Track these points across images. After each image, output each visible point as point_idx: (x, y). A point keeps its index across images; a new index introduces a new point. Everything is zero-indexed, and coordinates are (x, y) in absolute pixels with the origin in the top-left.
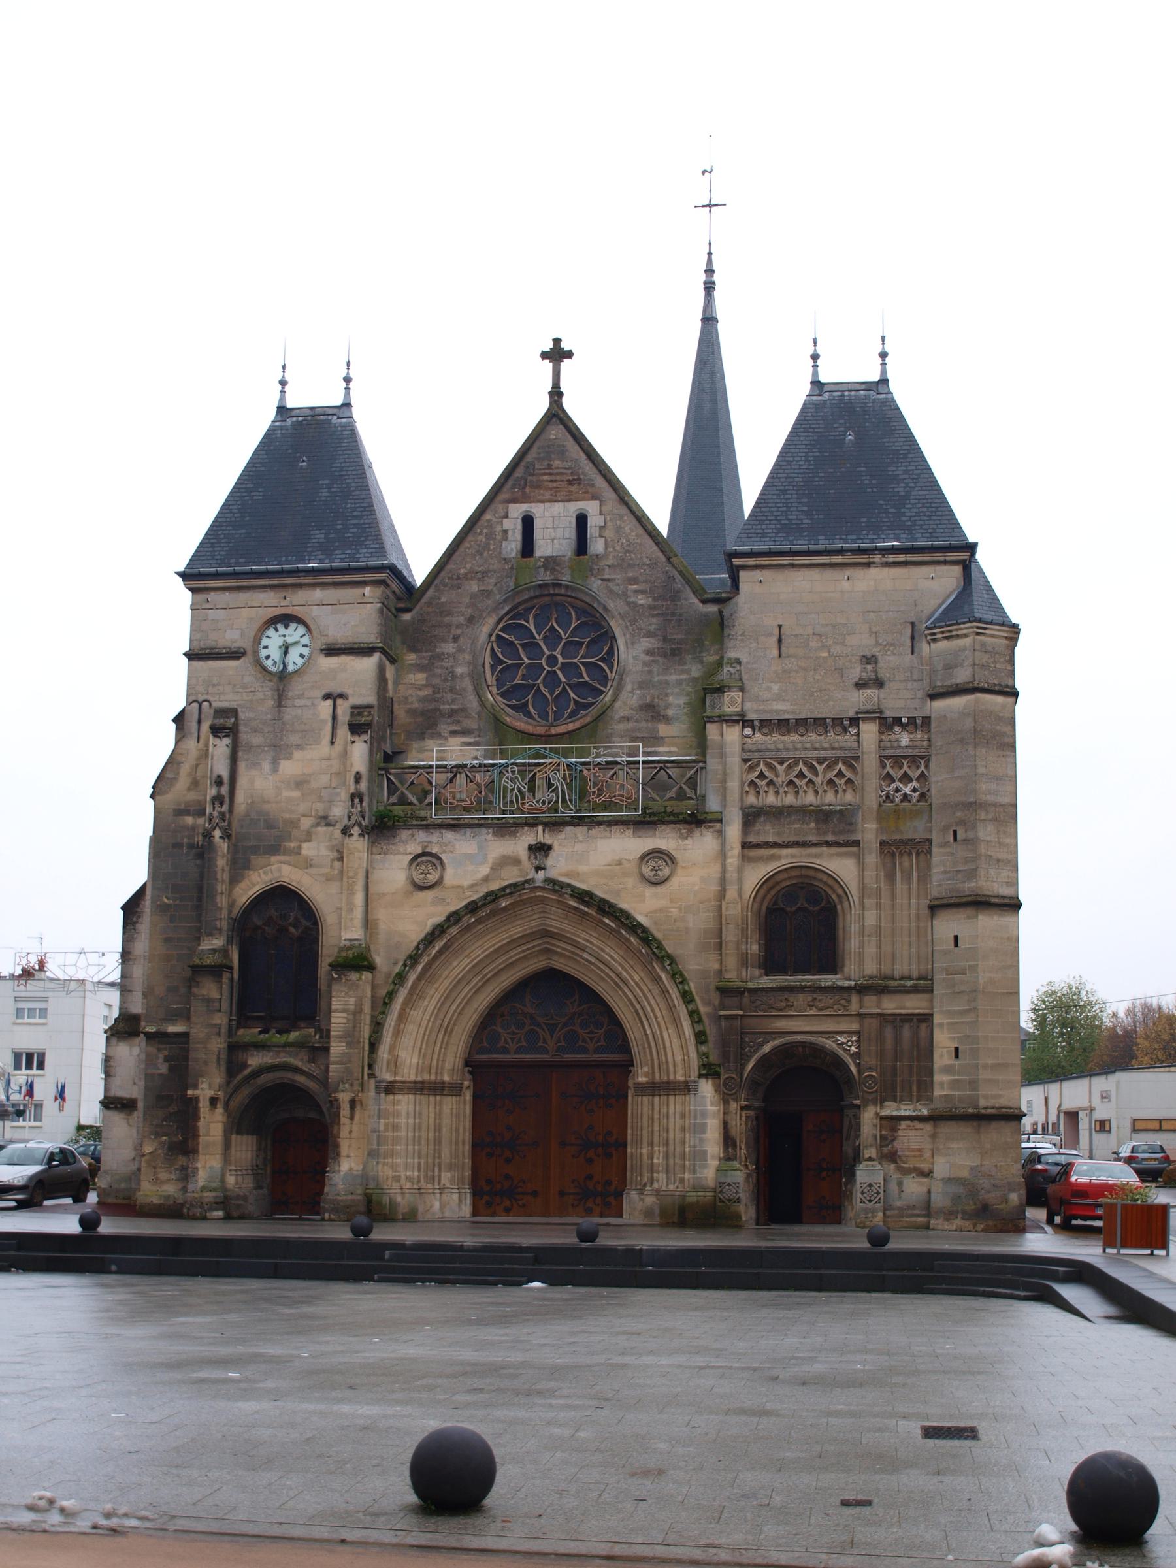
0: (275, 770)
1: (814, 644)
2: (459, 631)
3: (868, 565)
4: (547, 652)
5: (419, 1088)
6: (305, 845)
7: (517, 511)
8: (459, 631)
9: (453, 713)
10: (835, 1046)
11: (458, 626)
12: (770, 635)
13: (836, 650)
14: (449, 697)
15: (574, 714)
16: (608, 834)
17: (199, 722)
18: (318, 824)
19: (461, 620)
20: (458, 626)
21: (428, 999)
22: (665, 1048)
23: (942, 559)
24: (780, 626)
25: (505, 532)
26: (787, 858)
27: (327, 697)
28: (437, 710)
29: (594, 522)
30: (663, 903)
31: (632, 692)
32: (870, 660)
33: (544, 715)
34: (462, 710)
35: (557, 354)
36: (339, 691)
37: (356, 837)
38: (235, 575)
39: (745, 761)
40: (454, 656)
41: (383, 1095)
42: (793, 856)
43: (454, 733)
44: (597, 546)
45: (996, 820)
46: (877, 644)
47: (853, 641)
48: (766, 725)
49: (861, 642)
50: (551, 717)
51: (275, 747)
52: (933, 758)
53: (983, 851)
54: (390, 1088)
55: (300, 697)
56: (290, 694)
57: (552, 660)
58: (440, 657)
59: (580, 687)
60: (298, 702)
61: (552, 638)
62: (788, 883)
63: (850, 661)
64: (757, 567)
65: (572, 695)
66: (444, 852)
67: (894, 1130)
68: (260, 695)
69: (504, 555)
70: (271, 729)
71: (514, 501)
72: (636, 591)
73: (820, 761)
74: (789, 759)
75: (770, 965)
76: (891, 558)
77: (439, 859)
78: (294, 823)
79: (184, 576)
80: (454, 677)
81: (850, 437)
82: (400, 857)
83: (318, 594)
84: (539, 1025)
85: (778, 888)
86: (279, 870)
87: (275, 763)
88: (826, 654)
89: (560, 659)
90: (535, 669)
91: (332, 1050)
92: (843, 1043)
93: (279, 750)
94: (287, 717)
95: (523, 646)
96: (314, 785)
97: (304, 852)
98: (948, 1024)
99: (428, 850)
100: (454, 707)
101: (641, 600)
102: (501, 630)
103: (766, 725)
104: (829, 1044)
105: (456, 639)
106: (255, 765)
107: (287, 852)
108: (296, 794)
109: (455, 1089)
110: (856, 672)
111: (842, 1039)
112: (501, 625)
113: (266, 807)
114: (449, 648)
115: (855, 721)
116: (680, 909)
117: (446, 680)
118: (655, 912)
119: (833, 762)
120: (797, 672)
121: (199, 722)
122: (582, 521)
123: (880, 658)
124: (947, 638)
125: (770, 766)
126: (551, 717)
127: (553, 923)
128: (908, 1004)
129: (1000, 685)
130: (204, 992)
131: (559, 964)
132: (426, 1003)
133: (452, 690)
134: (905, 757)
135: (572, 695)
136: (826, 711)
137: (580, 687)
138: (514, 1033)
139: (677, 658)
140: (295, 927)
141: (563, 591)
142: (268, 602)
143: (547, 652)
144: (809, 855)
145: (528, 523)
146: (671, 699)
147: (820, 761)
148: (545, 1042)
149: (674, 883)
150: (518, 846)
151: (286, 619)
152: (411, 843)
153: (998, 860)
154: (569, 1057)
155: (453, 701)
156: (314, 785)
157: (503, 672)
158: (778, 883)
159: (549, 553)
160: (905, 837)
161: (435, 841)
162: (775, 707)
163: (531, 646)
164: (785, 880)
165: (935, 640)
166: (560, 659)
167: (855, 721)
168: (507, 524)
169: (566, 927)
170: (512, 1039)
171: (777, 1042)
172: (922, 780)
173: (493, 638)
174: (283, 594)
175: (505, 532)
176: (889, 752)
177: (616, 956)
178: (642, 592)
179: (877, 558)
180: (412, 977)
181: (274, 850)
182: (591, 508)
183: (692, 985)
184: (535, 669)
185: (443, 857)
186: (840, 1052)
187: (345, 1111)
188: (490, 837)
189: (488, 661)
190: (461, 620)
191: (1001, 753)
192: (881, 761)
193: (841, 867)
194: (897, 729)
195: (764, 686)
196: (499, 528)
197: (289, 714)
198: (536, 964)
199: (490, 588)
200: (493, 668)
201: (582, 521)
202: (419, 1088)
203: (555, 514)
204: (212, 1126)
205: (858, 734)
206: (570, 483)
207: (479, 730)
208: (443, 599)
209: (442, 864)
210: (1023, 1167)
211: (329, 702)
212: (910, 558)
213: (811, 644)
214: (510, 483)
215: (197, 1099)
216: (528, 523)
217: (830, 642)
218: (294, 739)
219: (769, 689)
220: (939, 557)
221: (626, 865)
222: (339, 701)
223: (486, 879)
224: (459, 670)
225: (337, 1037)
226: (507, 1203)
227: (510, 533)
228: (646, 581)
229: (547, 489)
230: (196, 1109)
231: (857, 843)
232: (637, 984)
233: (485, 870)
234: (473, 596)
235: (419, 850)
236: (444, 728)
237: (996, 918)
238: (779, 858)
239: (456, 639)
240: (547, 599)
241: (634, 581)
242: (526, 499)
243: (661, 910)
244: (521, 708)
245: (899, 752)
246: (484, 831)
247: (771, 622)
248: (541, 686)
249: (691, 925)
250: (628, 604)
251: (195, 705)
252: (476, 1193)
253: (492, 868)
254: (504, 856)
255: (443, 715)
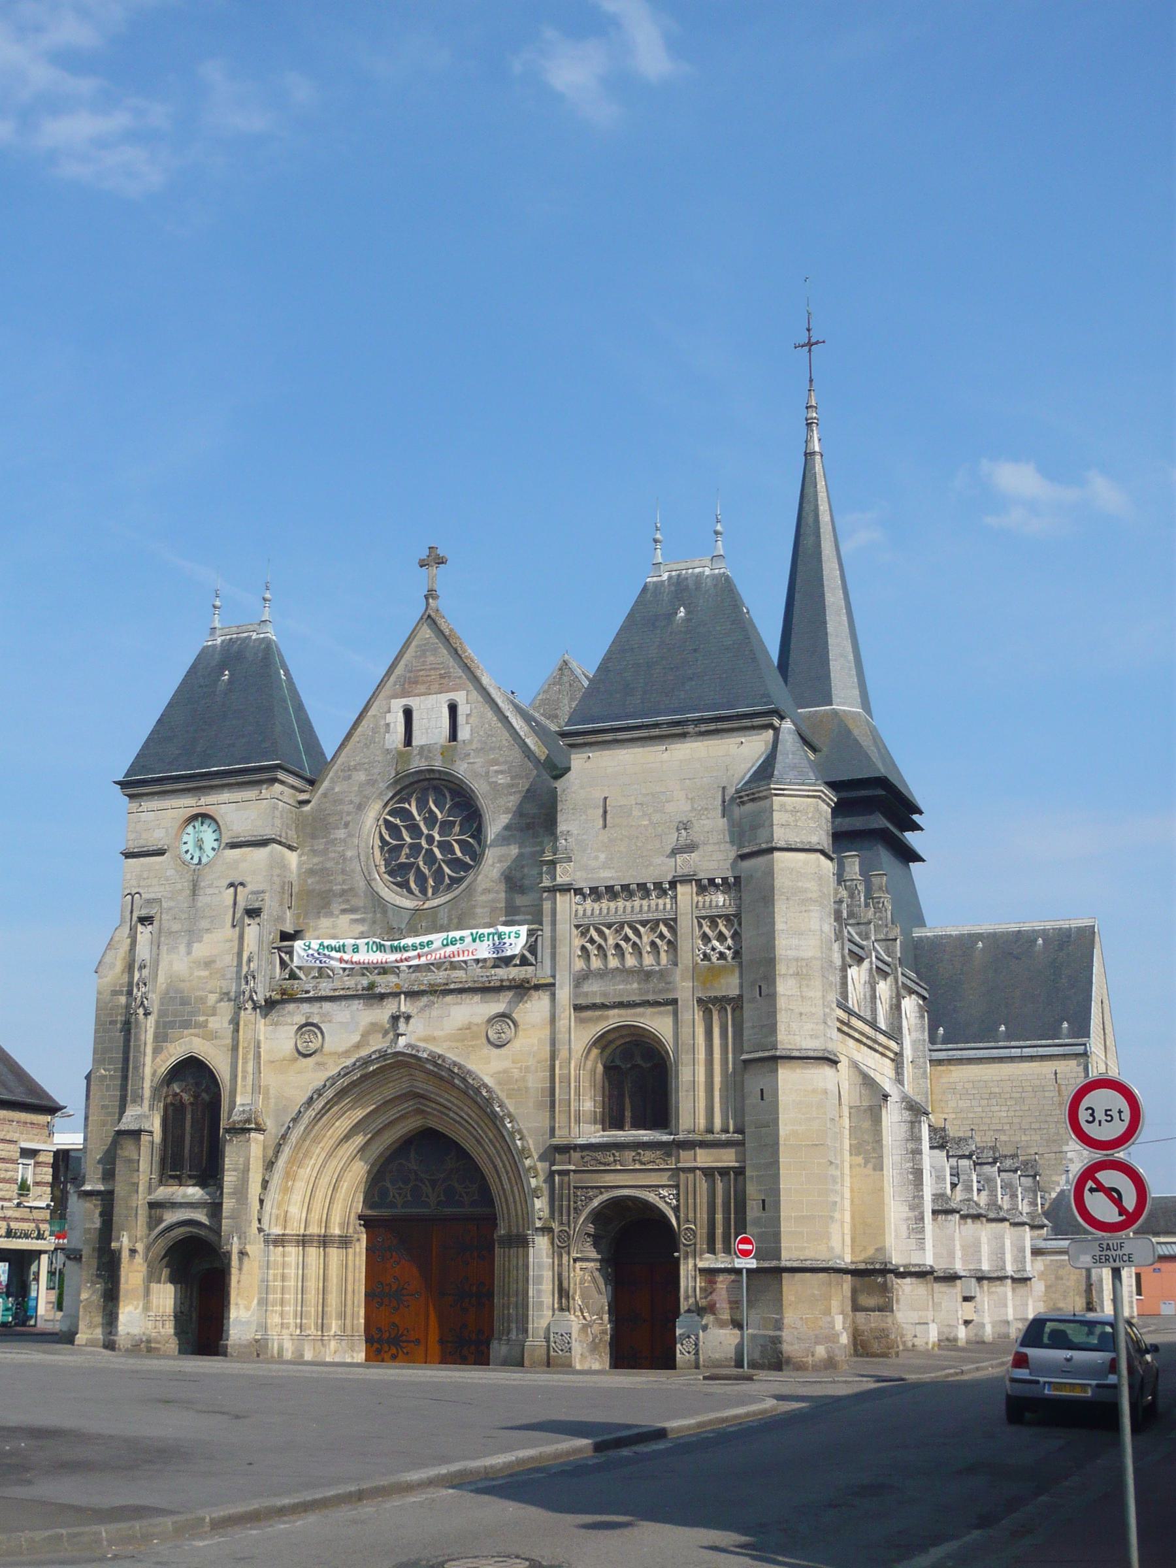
0: (189, 953)
1: (636, 813)
2: (349, 818)
3: (684, 735)
4: (425, 831)
5: (303, 1241)
6: (211, 1019)
7: (398, 705)
8: (349, 818)
9: (343, 893)
10: (657, 1198)
11: (349, 814)
12: (596, 807)
13: (656, 817)
14: (340, 878)
15: (449, 887)
16: (459, 1000)
17: (132, 912)
18: (221, 1000)
19: (351, 808)
20: (349, 814)
21: (314, 1157)
22: (515, 1202)
23: (749, 724)
24: (605, 799)
25: (388, 725)
26: (615, 1018)
27: (231, 885)
28: (331, 890)
29: (462, 710)
30: (507, 1064)
31: (493, 865)
32: (685, 826)
33: (424, 891)
34: (351, 889)
35: (434, 559)
36: (240, 880)
37: (249, 1011)
38: (177, 779)
39: (577, 927)
40: (344, 841)
41: (271, 1247)
42: (620, 1016)
43: (344, 911)
44: (464, 733)
45: (798, 974)
46: (693, 809)
47: (670, 808)
48: (595, 893)
49: (679, 807)
50: (430, 891)
51: (190, 932)
52: (743, 916)
53: (783, 1006)
54: (280, 1241)
55: (210, 886)
56: (202, 884)
57: (430, 839)
58: (333, 842)
59: (455, 863)
60: (209, 891)
61: (431, 820)
62: (623, 1041)
63: (669, 827)
64: (585, 745)
65: (447, 870)
66: (323, 1022)
67: (712, 1282)
68: (179, 886)
69: (387, 746)
70: (186, 916)
71: (395, 696)
72: (497, 772)
73: (644, 923)
74: (615, 923)
75: (613, 1120)
76: (703, 728)
77: (319, 1028)
78: (203, 1000)
79: (123, 784)
80: (345, 859)
81: (682, 613)
82: (286, 1027)
83: (226, 796)
84: (421, 1181)
85: (613, 1046)
86: (191, 1042)
87: (189, 945)
88: (646, 823)
89: (437, 837)
90: (415, 849)
91: (225, 1206)
92: (664, 1197)
93: (193, 935)
94: (199, 904)
95: (406, 827)
96: (219, 965)
97: (210, 1025)
98: (758, 1176)
99: (310, 1020)
100: (345, 887)
101: (501, 780)
102: (390, 813)
103: (595, 893)
104: (651, 1197)
105: (346, 825)
106: (173, 949)
107: (198, 1025)
108: (206, 973)
109: (345, 1242)
110: (671, 840)
111: (664, 1192)
112: (387, 810)
113: (182, 985)
114: (341, 833)
115: (673, 884)
116: (521, 1069)
117: (338, 863)
118: (499, 1073)
119: (654, 925)
120: (621, 840)
121: (132, 912)
122: (453, 709)
123: (695, 822)
124: (753, 800)
125: (601, 933)
126: (430, 891)
127: (420, 1085)
128: (724, 1158)
129: (802, 843)
130: (126, 1154)
131: (432, 1124)
132: (313, 1161)
133: (343, 872)
134: (720, 917)
135: (447, 870)
136: (648, 876)
137: (455, 863)
138: (401, 1189)
139: (531, 832)
140: (207, 1092)
141: (437, 776)
142: (186, 804)
143: (425, 831)
144: (634, 1015)
145: (408, 713)
146: (526, 870)
147: (644, 923)
148: (427, 1196)
149: (517, 1045)
150: (382, 1014)
151: (204, 817)
152: (297, 1014)
153: (801, 1014)
154: (449, 1211)
155: (344, 882)
156: (219, 965)
157: (391, 851)
158: (611, 1042)
159: (423, 742)
160: (719, 994)
161: (312, 1011)
162: (602, 875)
163: (414, 829)
164: (617, 1038)
165: (743, 803)
166: (437, 837)
167: (673, 884)
168: (389, 718)
169: (430, 1088)
170: (400, 1194)
171: (606, 1196)
172: (737, 938)
173: (381, 822)
174: (585, 756)
175: (388, 725)
176: (704, 913)
177: (473, 1115)
178: (501, 772)
179: (691, 729)
180: (294, 1137)
181: (186, 1025)
182: (460, 697)
183: (530, 1142)
184: (415, 849)
185: (322, 1026)
186: (662, 1205)
187: (235, 1262)
188: (361, 1007)
189: (378, 843)
190: (351, 808)
191: (804, 908)
192: (699, 922)
193: (659, 1024)
194: (712, 889)
195: (593, 855)
196: (382, 723)
197: (202, 900)
198: (412, 1124)
199: (374, 777)
200: (382, 848)
201: (453, 709)
202: (303, 1241)
203: (429, 706)
204: (132, 1273)
205: (675, 897)
206: (442, 677)
207: (365, 907)
208: (337, 790)
209: (322, 1033)
210: (1035, 1333)
211: (232, 889)
212: (720, 725)
213: (634, 813)
214: (393, 679)
215: (120, 1251)
216: (408, 713)
217: (651, 810)
218: (204, 924)
219: (596, 858)
220: (746, 723)
221: (474, 1028)
222: (240, 888)
223: (358, 1046)
224: (349, 854)
225: (229, 1194)
226: (394, 1351)
227: (392, 725)
228: (506, 762)
229: (424, 683)
230: (119, 1259)
231: (674, 1002)
232: (490, 1141)
233: (356, 1038)
234: (361, 785)
235: (303, 1022)
236: (336, 907)
237: (798, 1071)
238: (607, 1018)
239: (346, 825)
240: (426, 783)
241: (495, 762)
242: (404, 694)
243: (505, 1071)
244: (404, 885)
245: (714, 912)
246: (357, 1002)
247: (598, 795)
248: (421, 863)
249: (530, 1085)
250: (490, 783)
251: (129, 897)
252: (369, 1340)
253: (362, 1036)
254: (372, 1024)
255: (335, 896)
